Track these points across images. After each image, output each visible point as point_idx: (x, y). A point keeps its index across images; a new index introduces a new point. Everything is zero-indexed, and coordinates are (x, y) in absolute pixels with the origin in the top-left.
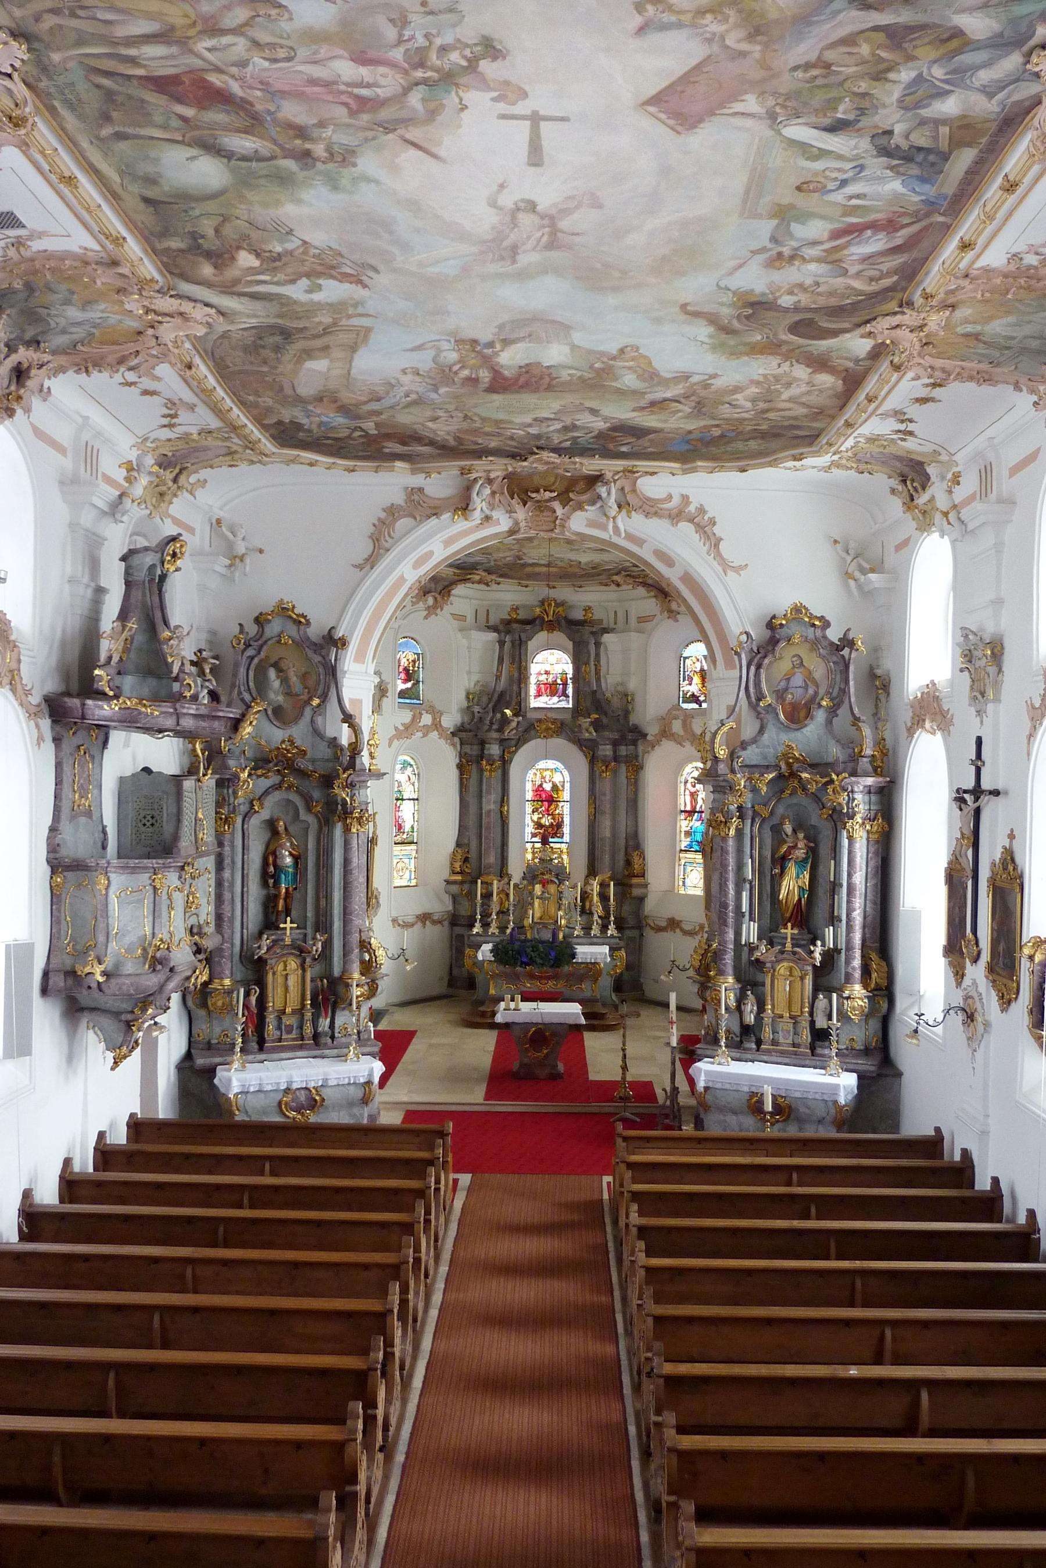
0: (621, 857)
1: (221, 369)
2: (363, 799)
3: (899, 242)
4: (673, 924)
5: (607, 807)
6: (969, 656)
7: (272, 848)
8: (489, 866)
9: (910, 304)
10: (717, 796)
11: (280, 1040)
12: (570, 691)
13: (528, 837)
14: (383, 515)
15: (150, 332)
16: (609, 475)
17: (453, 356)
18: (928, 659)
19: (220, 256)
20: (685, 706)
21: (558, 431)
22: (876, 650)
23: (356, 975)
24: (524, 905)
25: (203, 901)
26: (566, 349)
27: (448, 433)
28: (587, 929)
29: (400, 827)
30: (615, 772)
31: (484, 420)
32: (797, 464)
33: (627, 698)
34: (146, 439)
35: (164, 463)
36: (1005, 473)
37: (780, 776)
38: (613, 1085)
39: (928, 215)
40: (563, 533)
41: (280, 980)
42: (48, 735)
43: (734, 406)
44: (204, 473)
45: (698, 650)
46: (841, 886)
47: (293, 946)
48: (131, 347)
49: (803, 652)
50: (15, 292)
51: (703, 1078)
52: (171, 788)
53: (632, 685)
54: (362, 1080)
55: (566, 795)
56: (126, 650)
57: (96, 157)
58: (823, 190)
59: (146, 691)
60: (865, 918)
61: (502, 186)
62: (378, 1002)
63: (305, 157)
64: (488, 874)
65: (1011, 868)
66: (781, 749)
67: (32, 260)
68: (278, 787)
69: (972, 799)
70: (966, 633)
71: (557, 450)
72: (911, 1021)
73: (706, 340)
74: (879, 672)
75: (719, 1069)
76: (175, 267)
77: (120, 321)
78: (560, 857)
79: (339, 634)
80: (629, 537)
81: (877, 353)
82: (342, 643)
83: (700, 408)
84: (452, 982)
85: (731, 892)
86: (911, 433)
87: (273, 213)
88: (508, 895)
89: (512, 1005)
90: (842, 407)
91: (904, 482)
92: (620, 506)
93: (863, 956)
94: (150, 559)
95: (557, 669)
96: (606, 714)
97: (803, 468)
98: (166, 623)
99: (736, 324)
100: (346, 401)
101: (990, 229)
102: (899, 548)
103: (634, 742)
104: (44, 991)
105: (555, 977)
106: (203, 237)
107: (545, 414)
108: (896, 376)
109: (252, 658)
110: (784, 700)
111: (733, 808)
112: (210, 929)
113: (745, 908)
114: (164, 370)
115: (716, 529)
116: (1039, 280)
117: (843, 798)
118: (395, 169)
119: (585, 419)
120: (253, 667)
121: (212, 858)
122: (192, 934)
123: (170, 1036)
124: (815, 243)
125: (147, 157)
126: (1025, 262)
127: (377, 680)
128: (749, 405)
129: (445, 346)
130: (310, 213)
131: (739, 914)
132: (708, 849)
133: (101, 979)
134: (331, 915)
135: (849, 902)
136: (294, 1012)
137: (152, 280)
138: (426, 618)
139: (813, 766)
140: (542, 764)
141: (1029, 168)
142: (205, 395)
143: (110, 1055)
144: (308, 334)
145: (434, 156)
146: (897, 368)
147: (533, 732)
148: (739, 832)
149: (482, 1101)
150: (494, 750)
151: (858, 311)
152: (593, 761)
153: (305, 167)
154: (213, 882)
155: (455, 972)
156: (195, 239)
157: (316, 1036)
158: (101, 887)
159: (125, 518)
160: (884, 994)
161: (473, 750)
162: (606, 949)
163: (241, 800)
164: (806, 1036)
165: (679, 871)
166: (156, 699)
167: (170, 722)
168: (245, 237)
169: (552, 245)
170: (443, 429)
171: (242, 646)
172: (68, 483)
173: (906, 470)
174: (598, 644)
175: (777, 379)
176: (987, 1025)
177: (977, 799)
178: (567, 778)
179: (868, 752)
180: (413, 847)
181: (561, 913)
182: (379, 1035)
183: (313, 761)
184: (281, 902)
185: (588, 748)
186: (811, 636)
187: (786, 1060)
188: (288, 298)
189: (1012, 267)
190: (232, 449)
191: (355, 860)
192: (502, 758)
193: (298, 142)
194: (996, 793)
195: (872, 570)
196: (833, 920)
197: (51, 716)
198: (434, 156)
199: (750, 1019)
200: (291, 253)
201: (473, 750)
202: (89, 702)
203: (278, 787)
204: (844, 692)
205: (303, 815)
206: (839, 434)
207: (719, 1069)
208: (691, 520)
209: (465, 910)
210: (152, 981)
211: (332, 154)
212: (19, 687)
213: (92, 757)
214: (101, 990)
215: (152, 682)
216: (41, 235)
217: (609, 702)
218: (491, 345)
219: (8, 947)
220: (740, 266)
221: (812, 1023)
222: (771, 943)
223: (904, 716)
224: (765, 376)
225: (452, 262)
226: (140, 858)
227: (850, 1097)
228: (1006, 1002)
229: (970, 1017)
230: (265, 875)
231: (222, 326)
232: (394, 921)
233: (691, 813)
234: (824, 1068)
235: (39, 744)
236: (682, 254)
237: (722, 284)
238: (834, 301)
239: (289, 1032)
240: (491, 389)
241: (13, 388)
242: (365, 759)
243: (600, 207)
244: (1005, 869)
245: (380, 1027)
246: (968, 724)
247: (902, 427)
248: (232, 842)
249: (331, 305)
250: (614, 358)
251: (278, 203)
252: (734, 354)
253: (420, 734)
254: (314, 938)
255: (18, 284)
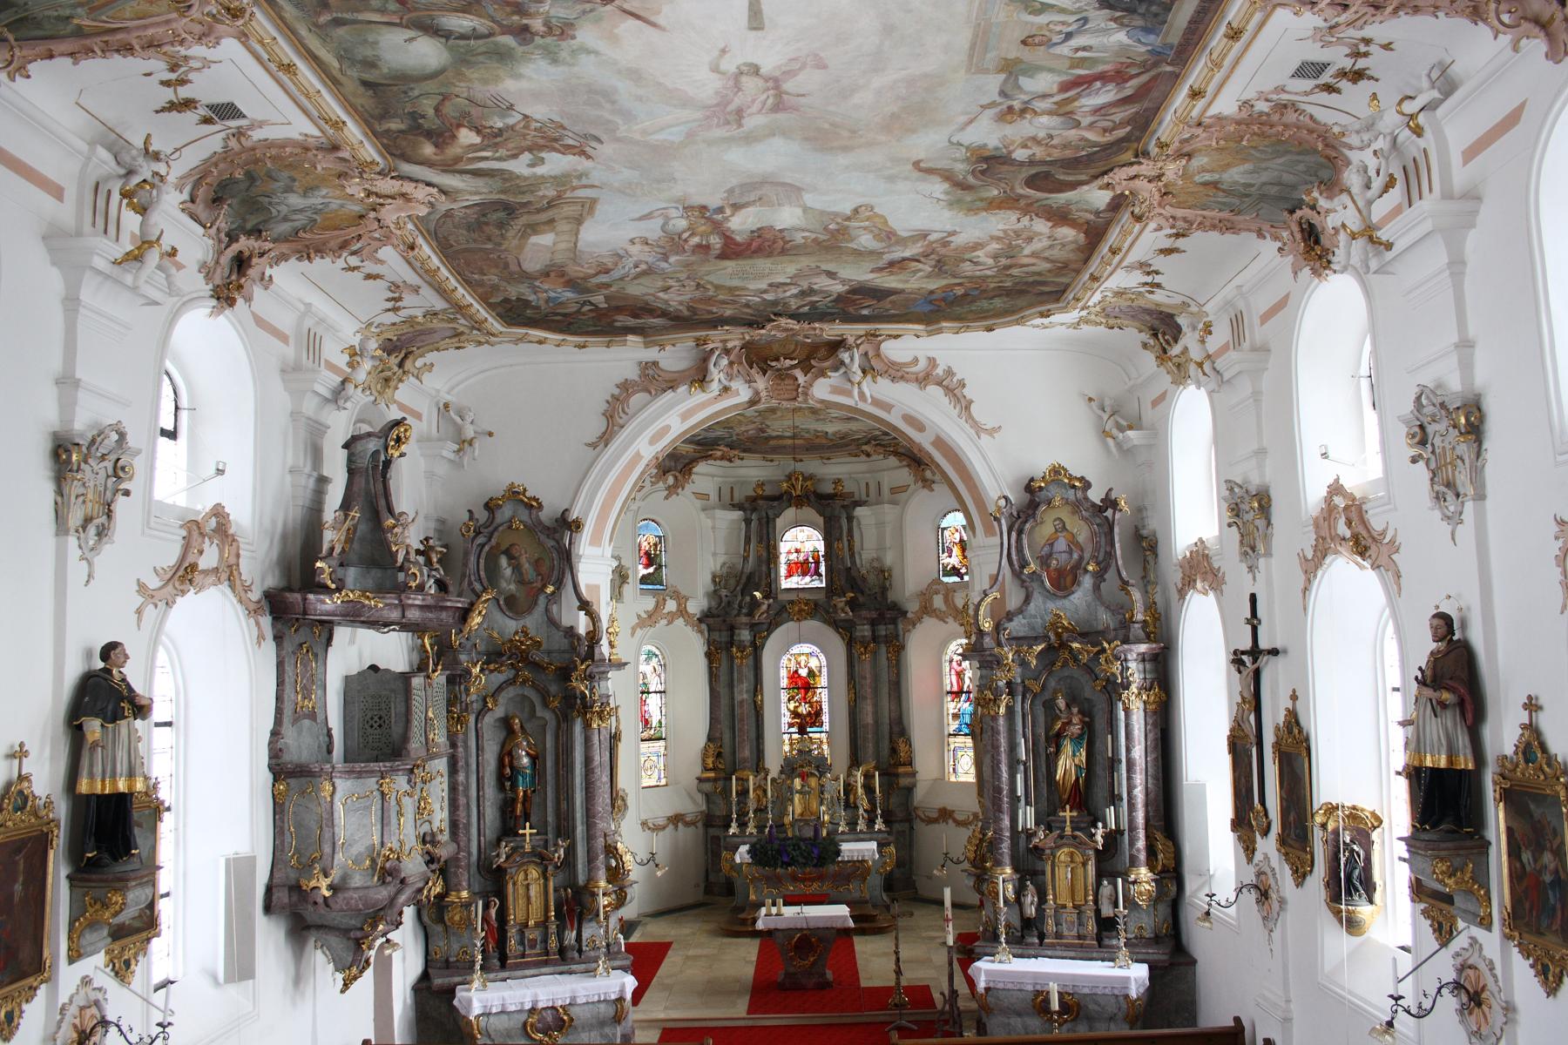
0: (885, 745)
1: (445, 249)
2: (603, 691)
3: (1128, 92)
4: (945, 815)
5: (868, 691)
6: (1236, 510)
7: (507, 748)
8: (745, 760)
9: (1146, 154)
10: (984, 672)
11: (523, 956)
12: (823, 569)
13: (784, 728)
14: (617, 391)
15: (372, 215)
16: (851, 340)
17: (683, 223)
18: (1194, 518)
19: (440, 135)
20: (946, 580)
21: (795, 296)
22: (1140, 510)
23: (602, 883)
24: (783, 799)
25: (436, 807)
26: (799, 211)
27: (681, 303)
28: (852, 824)
29: (647, 722)
30: (875, 653)
31: (717, 287)
32: (1046, 321)
33: (884, 574)
34: (371, 324)
35: (389, 347)
36: (1257, 321)
37: (1049, 648)
38: (887, 991)
39: (1156, 65)
40: (806, 401)
41: (521, 891)
42: (269, 633)
43: (976, 263)
44: (431, 357)
45: (956, 520)
46: (1120, 761)
47: (533, 853)
48: (353, 232)
49: (1065, 514)
50: (237, 182)
51: (983, 978)
52: (399, 685)
53: (889, 559)
54: (613, 997)
55: (823, 681)
56: (349, 540)
57: (314, 43)
58: (1049, 44)
59: (370, 583)
60: (1147, 795)
61: (723, 51)
62: (629, 912)
63: (523, 33)
64: (744, 769)
65: (1296, 731)
66: (1048, 618)
67: (253, 149)
68: (511, 682)
69: (1250, 661)
70: (1231, 485)
71: (796, 316)
72: (1201, 902)
73: (942, 197)
74: (1145, 532)
75: (1000, 968)
76: (396, 148)
77: (342, 206)
78: (820, 747)
79: (574, 515)
80: (876, 402)
81: (1117, 204)
82: (577, 526)
83: (940, 266)
84: (708, 890)
85: (1005, 775)
86: (1158, 286)
87: (492, 89)
88: (765, 791)
89: (774, 910)
90: (1086, 261)
91: (1155, 335)
92: (864, 372)
93: (1147, 837)
94: (372, 445)
95: (808, 547)
96: (862, 593)
97: (1052, 325)
98: (390, 511)
99: (971, 180)
100: (574, 275)
101: (1218, 77)
102: (1155, 403)
103: (894, 622)
104: (268, 909)
105: (821, 878)
106: (423, 117)
107: (782, 280)
108: (1138, 227)
109: (483, 546)
110: (1049, 566)
111: (1002, 684)
112: (445, 837)
113: (1020, 791)
114: (387, 253)
115: (966, 391)
116: (1272, 126)
117: (1116, 668)
118: (614, 39)
119: (822, 283)
120: (483, 555)
121: (445, 760)
122: (424, 842)
123: (405, 956)
124: (1045, 96)
125: (366, 41)
126: (1257, 108)
127: (615, 564)
128: (990, 261)
129: (673, 213)
130: (530, 87)
131: (1014, 799)
132: (978, 731)
133: (327, 894)
134: (574, 819)
135: (1129, 778)
136: (537, 925)
137: (373, 162)
138: (666, 498)
139: (1084, 636)
140: (796, 649)
141: (1252, 15)
142: (429, 275)
143: (340, 977)
144: (532, 208)
145: (654, 25)
146: (1138, 218)
147: (785, 615)
148: (1010, 710)
149: (744, 1015)
150: (745, 635)
151: (1093, 163)
152: (850, 644)
153: (524, 42)
154: (445, 786)
155: (712, 878)
156: (415, 119)
157: (562, 951)
158: (326, 794)
159: (348, 405)
160: (1171, 874)
161: (723, 637)
162: (873, 845)
163: (474, 697)
164: (1091, 926)
165: (948, 758)
166: (380, 590)
167: (395, 615)
168: (466, 114)
169: (778, 107)
170: (676, 299)
171: (472, 534)
172: (290, 371)
173: (1156, 323)
174: (850, 519)
175: (1017, 234)
176: (1282, 902)
177: (1255, 661)
178: (824, 663)
179: (1139, 617)
180: (662, 743)
181: (823, 808)
182: (630, 948)
183: (549, 653)
184: (519, 806)
185: (845, 629)
186: (1072, 498)
187: (1072, 954)
188: (511, 173)
189: (1244, 115)
190: (453, 330)
191: (597, 758)
192: (753, 644)
193: (516, 18)
194: (1274, 652)
195: (1130, 428)
196: (1114, 799)
197: (271, 613)
198: (654, 25)
199: (1031, 911)
200: (512, 128)
201: (723, 637)
202: (311, 596)
203: (511, 682)
204: (1110, 555)
205: (540, 712)
206: (1085, 288)
207: (1000, 968)
208: (940, 384)
209: (719, 810)
210: (383, 894)
211: (550, 28)
212: (238, 582)
213: (316, 655)
214: (327, 905)
215: (376, 573)
216: (261, 124)
217: (864, 579)
218: (720, 210)
219: (228, 860)
220: (971, 122)
221: (1098, 912)
222: (1049, 828)
223: (1174, 577)
224: (1005, 231)
225: (674, 129)
226: (368, 761)
227: (1142, 990)
228: (1300, 876)
229: (1263, 894)
230: (501, 778)
231: (444, 205)
232: (644, 824)
233: (957, 694)
234: (1113, 960)
235: (259, 643)
236: (914, 110)
237: (954, 140)
238: (1068, 153)
239: (533, 946)
240: (723, 256)
241: (234, 277)
242: (604, 648)
243: (825, 67)
244: (1290, 732)
245: (633, 940)
246: (1240, 581)
247: (1149, 279)
248: (465, 742)
249: (555, 178)
250: (848, 219)
251: (497, 79)
252: (972, 210)
253: (664, 622)
254: (556, 845)
255: (239, 174)
